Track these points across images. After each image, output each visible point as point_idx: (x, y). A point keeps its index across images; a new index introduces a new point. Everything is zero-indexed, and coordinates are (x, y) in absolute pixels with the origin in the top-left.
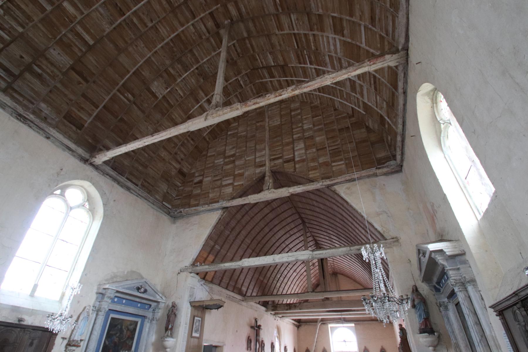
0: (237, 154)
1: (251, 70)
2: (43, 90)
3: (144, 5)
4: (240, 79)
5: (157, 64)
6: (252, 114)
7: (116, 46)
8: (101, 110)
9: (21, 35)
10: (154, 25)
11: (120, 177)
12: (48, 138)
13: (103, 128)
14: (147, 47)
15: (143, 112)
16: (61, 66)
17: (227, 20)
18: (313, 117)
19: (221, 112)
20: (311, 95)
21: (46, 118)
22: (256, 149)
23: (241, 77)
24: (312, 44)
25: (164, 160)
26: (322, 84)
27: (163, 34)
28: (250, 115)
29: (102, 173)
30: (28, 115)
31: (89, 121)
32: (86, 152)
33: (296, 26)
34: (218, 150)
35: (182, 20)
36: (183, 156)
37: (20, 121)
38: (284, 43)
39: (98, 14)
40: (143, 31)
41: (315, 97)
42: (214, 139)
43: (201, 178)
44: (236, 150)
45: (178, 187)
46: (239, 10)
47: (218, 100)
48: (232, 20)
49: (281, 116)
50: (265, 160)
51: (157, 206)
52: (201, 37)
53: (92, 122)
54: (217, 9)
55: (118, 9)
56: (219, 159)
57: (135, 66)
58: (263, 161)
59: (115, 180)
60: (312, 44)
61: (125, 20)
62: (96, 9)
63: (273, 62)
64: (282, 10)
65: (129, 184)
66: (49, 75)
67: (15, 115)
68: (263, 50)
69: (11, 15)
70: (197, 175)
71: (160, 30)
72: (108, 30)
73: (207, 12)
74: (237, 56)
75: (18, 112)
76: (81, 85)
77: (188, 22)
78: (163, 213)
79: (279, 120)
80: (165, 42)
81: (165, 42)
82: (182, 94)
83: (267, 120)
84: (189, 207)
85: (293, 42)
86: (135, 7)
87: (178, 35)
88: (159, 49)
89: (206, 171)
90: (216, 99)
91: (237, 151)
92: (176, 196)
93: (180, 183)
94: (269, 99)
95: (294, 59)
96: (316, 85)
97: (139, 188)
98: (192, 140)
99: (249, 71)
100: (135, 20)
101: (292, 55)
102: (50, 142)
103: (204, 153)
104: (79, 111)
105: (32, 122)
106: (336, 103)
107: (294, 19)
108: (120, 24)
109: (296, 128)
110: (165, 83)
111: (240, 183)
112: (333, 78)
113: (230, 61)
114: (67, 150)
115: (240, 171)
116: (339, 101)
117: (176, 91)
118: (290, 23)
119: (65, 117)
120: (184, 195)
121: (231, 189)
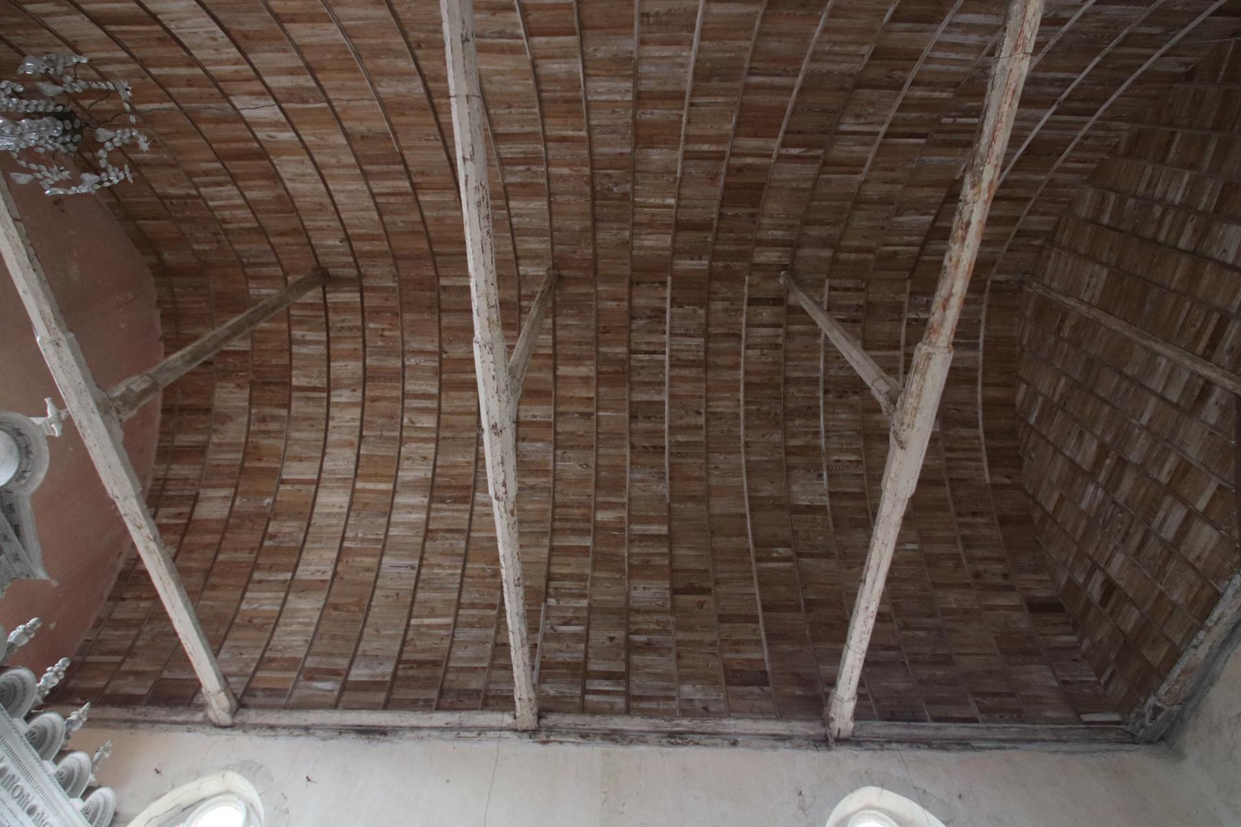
0: (1108, 439)
1: (910, 277)
2: (664, 663)
3: (670, 407)
4: (913, 316)
5: (766, 459)
6: (1027, 334)
7: (694, 498)
8: (764, 618)
9: (590, 609)
10: (706, 413)
11: (916, 727)
12: (735, 744)
13: (797, 648)
14: (729, 453)
15: (827, 555)
16: (660, 603)
17: (779, 277)
18: (1163, 160)
19: (910, 400)
20: (1086, 142)
21: (705, 708)
22: (1132, 380)
23: (909, 311)
24: (937, 94)
25: (967, 612)
26: (1012, 87)
27: (729, 410)
28: (1025, 342)
29: (876, 747)
30: (678, 725)
31: (766, 656)
32: (809, 720)
33: (871, 123)
34: (1054, 479)
35: (728, 360)
36: (1001, 566)
37: (678, 744)
38: (892, 170)
39: (638, 484)
40: (702, 439)
41: (1101, 133)
42: (1020, 467)
43: (1098, 578)
44: (1093, 433)
45: (1075, 647)
46: (774, 243)
47: (885, 388)
48: (785, 267)
49: (1091, 257)
50: (1192, 373)
51: (1077, 741)
52: (776, 346)
53: (770, 653)
54: (751, 286)
55: (651, 450)
56: (1083, 496)
57: (743, 497)
58: (1189, 382)
59: (915, 742)
60: (937, 94)
61: (671, 454)
62: (632, 481)
63: (924, 215)
64: (820, 147)
65: (952, 730)
66: (659, 632)
67: (666, 740)
68: (883, 228)
69: (563, 595)
70: (1081, 579)
71: (720, 410)
72: (666, 491)
73: (745, 308)
74: (859, 293)
75: (663, 732)
76: (706, 606)
77: (738, 353)
78: (1114, 747)
79: (1097, 267)
80: (742, 416)
81: (742, 416)
82: (854, 458)
83: (1071, 302)
84: (1163, 679)
85: (905, 145)
86: (664, 423)
87: (746, 385)
88: (746, 436)
89: (1091, 552)
90: (879, 391)
91: (1098, 433)
92: (1099, 674)
93: (1070, 634)
94: (958, 261)
95: (949, 159)
96: (1005, 107)
97: (984, 721)
98: (974, 514)
99: (908, 285)
100: (681, 438)
101: (936, 159)
102: (742, 750)
103: (1037, 515)
104: (737, 651)
105: (693, 733)
106: (1162, 69)
107: (854, 124)
108: (671, 464)
109: (1159, 228)
110: (809, 471)
111: (1208, 494)
112: (1016, 48)
113: (860, 314)
114: (779, 744)
115: (1168, 466)
116: (1162, 56)
117: (839, 464)
118: (856, 137)
119: (728, 683)
120: (1113, 656)
121: (1208, 529)
